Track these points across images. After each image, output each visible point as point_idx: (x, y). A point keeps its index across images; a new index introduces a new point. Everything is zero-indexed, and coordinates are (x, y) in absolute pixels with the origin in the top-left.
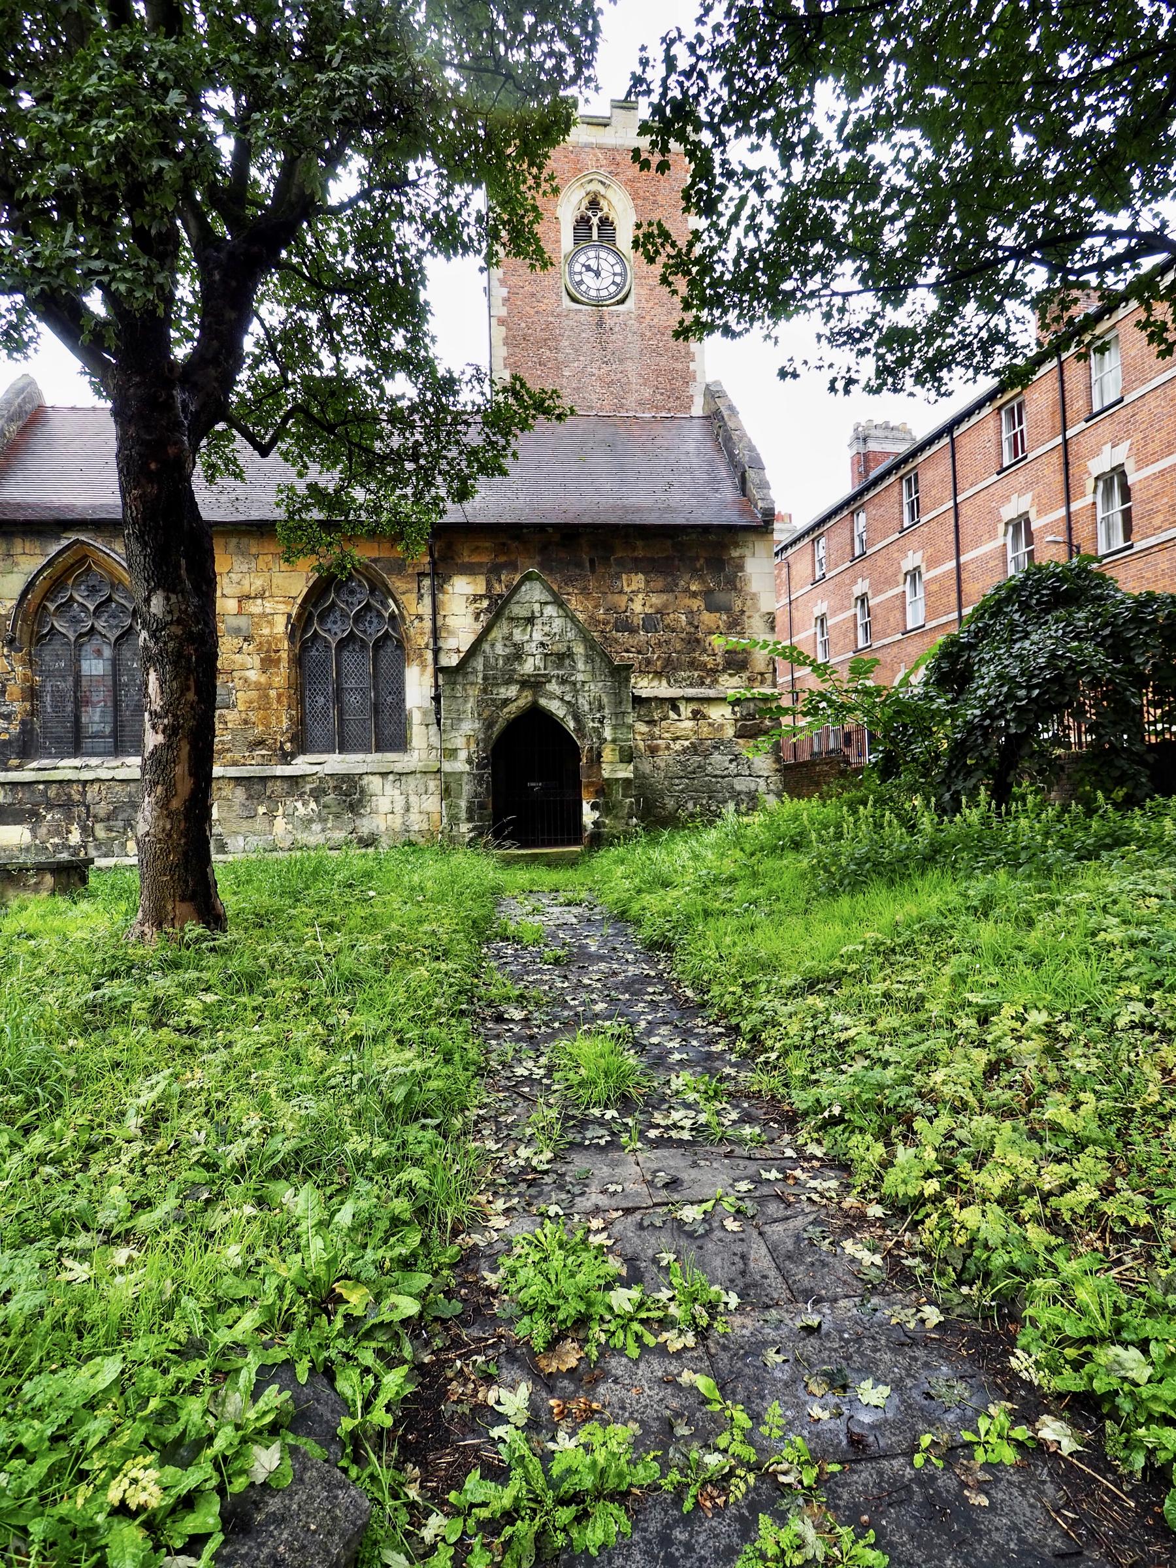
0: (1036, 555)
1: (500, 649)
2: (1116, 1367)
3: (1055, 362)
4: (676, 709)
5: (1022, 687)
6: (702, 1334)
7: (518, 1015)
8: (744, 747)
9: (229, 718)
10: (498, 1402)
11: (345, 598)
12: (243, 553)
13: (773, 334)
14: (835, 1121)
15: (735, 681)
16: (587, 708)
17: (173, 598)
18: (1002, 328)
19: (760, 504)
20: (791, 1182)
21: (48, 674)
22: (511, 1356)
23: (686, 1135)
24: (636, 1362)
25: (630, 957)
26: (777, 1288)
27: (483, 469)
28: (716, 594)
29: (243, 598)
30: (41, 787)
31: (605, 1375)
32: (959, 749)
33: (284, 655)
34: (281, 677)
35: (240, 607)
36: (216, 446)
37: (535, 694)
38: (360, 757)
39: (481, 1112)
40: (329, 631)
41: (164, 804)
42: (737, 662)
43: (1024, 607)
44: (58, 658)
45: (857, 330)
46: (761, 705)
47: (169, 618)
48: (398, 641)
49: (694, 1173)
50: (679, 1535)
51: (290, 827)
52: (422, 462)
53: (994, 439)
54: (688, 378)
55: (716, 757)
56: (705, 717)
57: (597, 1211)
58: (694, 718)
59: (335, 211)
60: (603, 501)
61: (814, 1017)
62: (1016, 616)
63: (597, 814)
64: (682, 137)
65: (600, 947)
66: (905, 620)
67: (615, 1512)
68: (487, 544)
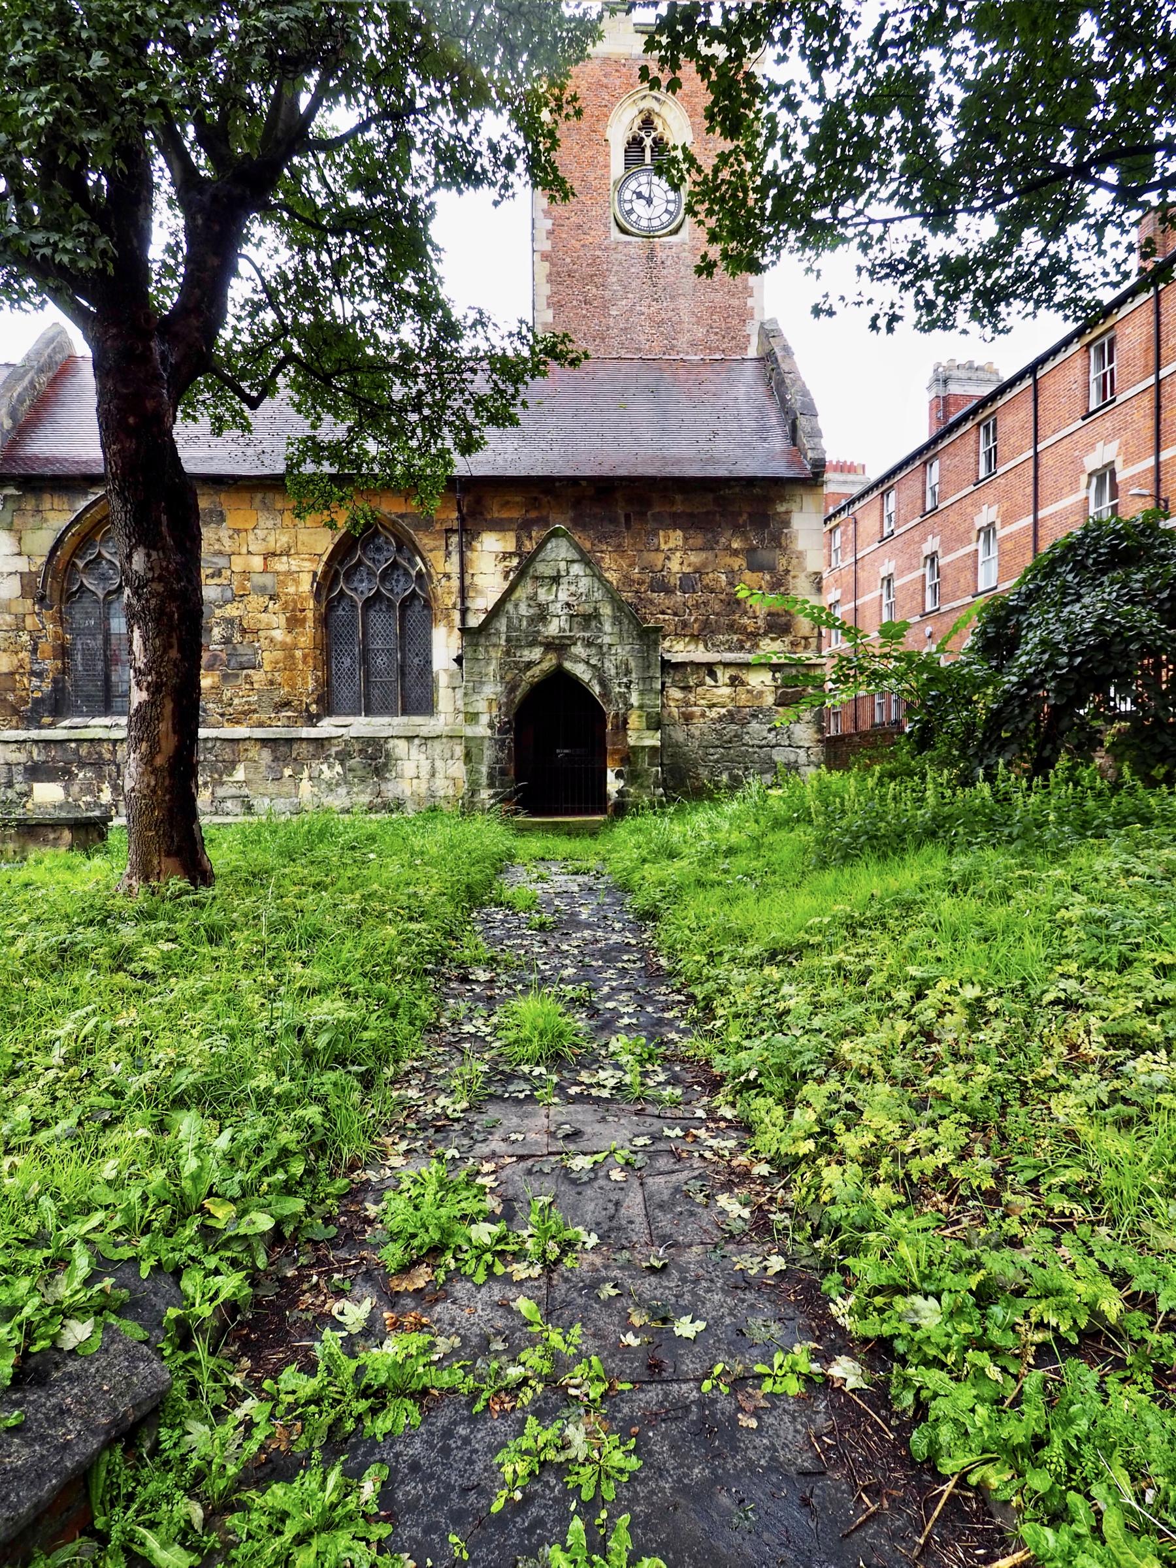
0: (1121, 509)
1: (523, 610)
2: (912, 1314)
3: (1152, 292)
4: (712, 674)
5: (1064, 654)
6: (550, 1267)
7: (483, 976)
8: (782, 717)
9: (255, 678)
10: (341, 1313)
11: (371, 555)
12: (267, 508)
13: (815, 267)
14: (749, 1085)
15: (777, 646)
16: (613, 672)
17: (154, 555)
18: (1064, 256)
19: (810, 454)
20: (689, 1139)
21: (78, 633)
22: (368, 1276)
23: (605, 1093)
24: (479, 1287)
25: (618, 926)
26: (639, 1231)
27: (494, 420)
28: (759, 551)
29: (269, 555)
30: (73, 745)
31: (447, 1295)
32: (996, 719)
33: (310, 614)
34: (306, 637)
35: (265, 565)
36: (221, 398)
37: (559, 657)
38: (386, 720)
39: (416, 1064)
40: (355, 590)
41: (148, 760)
42: (779, 625)
43: (1079, 567)
44: (88, 616)
45: (901, 261)
46: (804, 671)
47: (150, 575)
48: (426, 600)
49: (598, 1127)
50: (462, 1430)
51: (315, 790)
52: (426, 412)
53: (1081, 379)
54: (745, 315)
55: (754, 726)
56: (743, 683)
57: (493, 1155)
58: (732, 685)
59: (329, 145)
60: (642, 451)
61: (764, 986)
62: (1070, 577)
63: (621, 783)
64: (692, 52)
65: (590, 916)
66: (976, 582)
67: (410, 1408)
68: (518, 499)
